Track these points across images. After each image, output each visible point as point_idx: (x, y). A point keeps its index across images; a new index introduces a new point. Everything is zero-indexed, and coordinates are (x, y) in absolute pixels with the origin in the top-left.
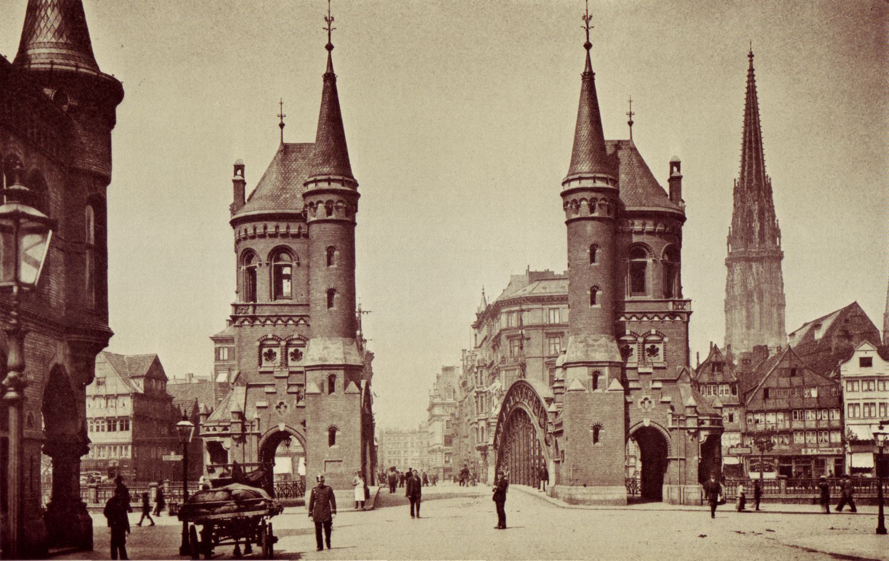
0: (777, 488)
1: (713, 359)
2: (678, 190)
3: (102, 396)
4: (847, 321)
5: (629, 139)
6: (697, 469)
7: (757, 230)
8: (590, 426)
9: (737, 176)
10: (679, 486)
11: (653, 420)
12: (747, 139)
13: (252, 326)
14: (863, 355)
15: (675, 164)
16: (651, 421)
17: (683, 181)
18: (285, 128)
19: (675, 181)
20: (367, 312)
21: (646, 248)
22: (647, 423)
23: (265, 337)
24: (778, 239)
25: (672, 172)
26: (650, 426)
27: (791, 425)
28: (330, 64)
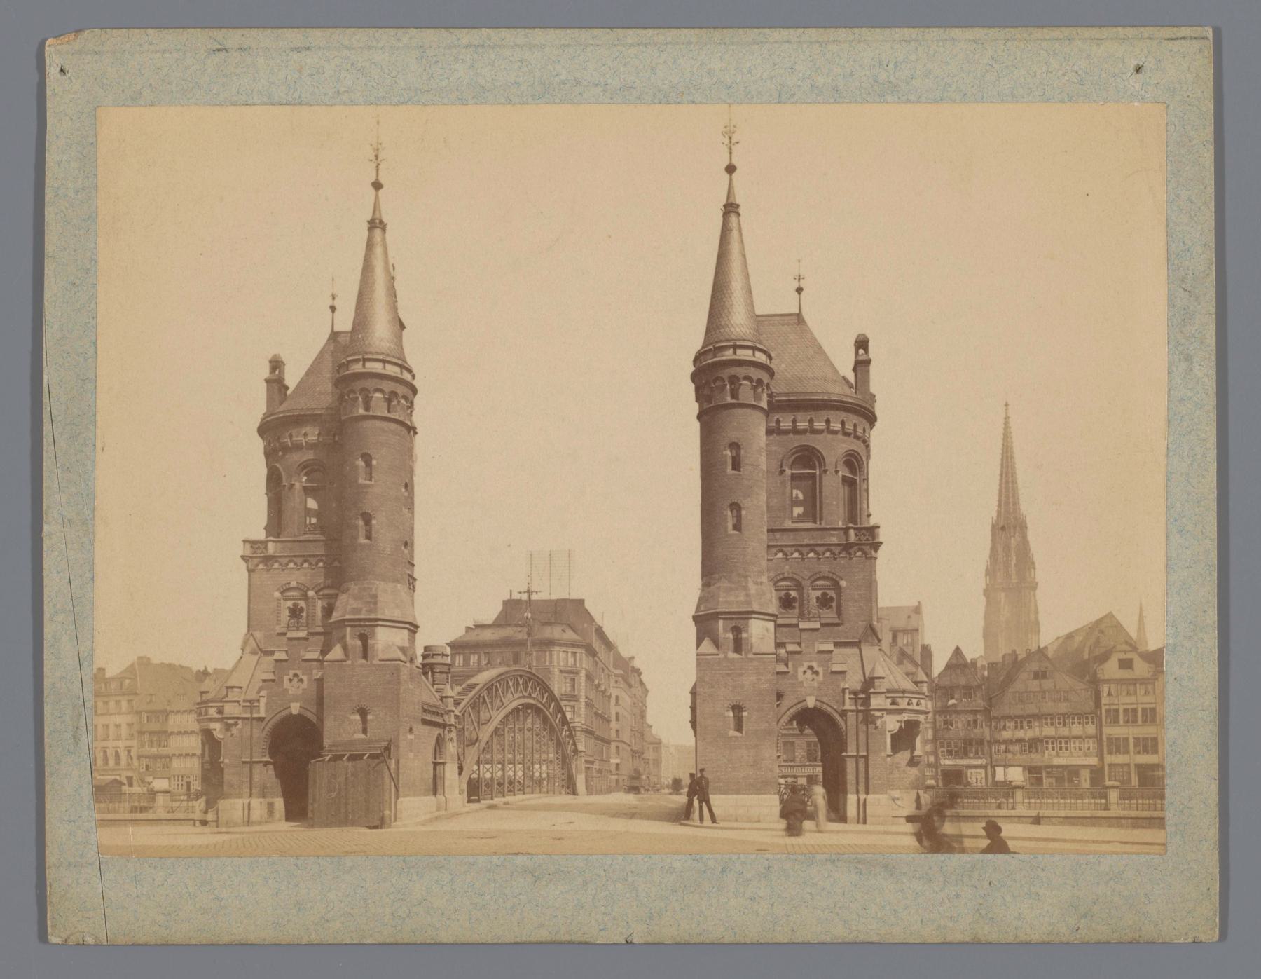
0: (1104, 801)
1: (954, 661)
2: (866, 381)
3: (596, 738)
4: (1102, 632)
5: (797, 311)
6: (45, 637)
7: (1013, 563)
8: (726, 705)
9: (994, 514)
10: (246, 801)
11: (819, 698)
12: (1004, 481)
13: (268, 570)
14: (1123, 656)
15: (862, 344)
16: (817, 700)
17: (873, 367)
18: (336, 312)
19: (862, 365)
20: (537, 593)
21: (820, 463)
22: (811, 702)
23: (287, 586)
24: (1033, 570)
25: (857, 353)
26: (815, 709)
27: (1041, 731)
28: (376, 207)
